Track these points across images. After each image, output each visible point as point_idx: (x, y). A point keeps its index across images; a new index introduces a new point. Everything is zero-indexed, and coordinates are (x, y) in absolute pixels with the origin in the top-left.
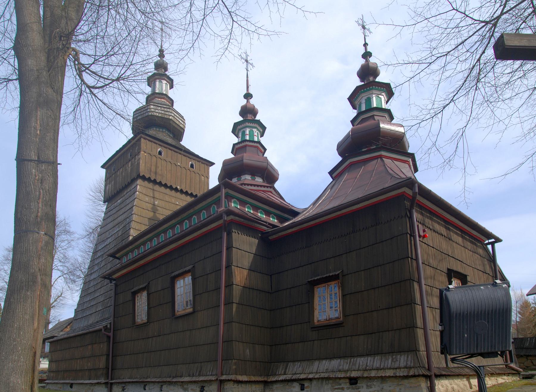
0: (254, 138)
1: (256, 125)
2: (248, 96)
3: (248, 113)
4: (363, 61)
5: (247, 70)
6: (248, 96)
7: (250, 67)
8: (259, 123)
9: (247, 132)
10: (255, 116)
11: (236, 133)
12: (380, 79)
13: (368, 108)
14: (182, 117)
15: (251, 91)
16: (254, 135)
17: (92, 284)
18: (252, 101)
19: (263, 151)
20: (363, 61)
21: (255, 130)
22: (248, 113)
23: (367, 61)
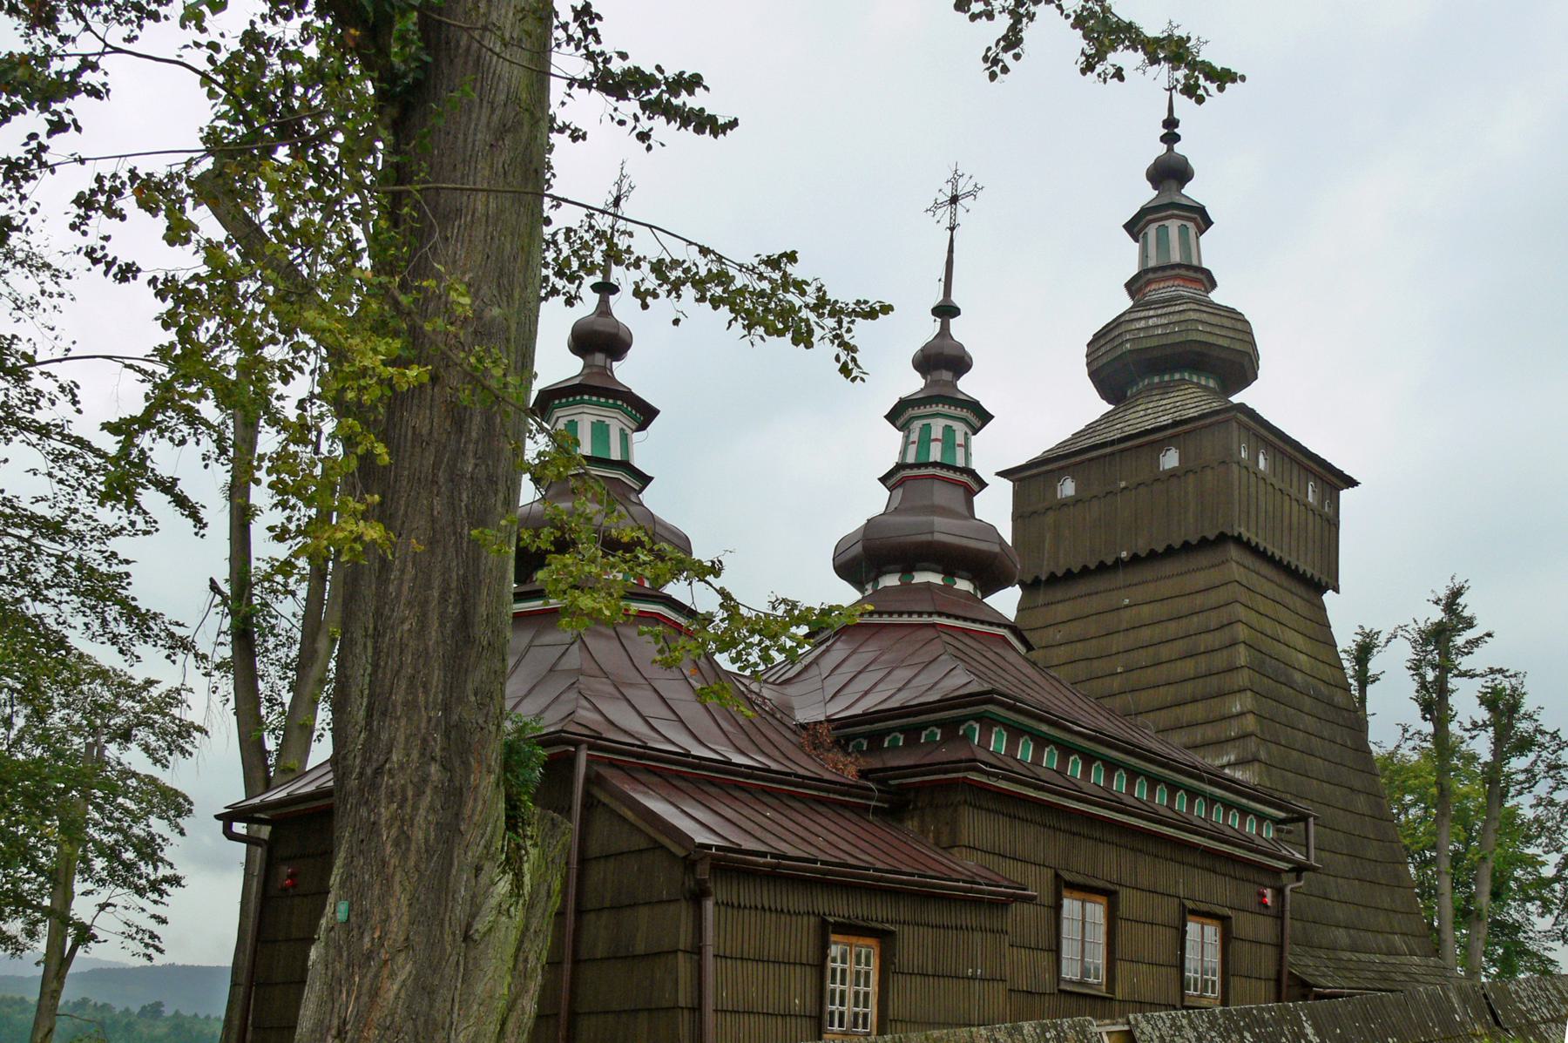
1: (964, 413)
2: (946, 311)
9: (937, 432)
13: (922, 460)
20: (933, 327)
23: (945, 331)
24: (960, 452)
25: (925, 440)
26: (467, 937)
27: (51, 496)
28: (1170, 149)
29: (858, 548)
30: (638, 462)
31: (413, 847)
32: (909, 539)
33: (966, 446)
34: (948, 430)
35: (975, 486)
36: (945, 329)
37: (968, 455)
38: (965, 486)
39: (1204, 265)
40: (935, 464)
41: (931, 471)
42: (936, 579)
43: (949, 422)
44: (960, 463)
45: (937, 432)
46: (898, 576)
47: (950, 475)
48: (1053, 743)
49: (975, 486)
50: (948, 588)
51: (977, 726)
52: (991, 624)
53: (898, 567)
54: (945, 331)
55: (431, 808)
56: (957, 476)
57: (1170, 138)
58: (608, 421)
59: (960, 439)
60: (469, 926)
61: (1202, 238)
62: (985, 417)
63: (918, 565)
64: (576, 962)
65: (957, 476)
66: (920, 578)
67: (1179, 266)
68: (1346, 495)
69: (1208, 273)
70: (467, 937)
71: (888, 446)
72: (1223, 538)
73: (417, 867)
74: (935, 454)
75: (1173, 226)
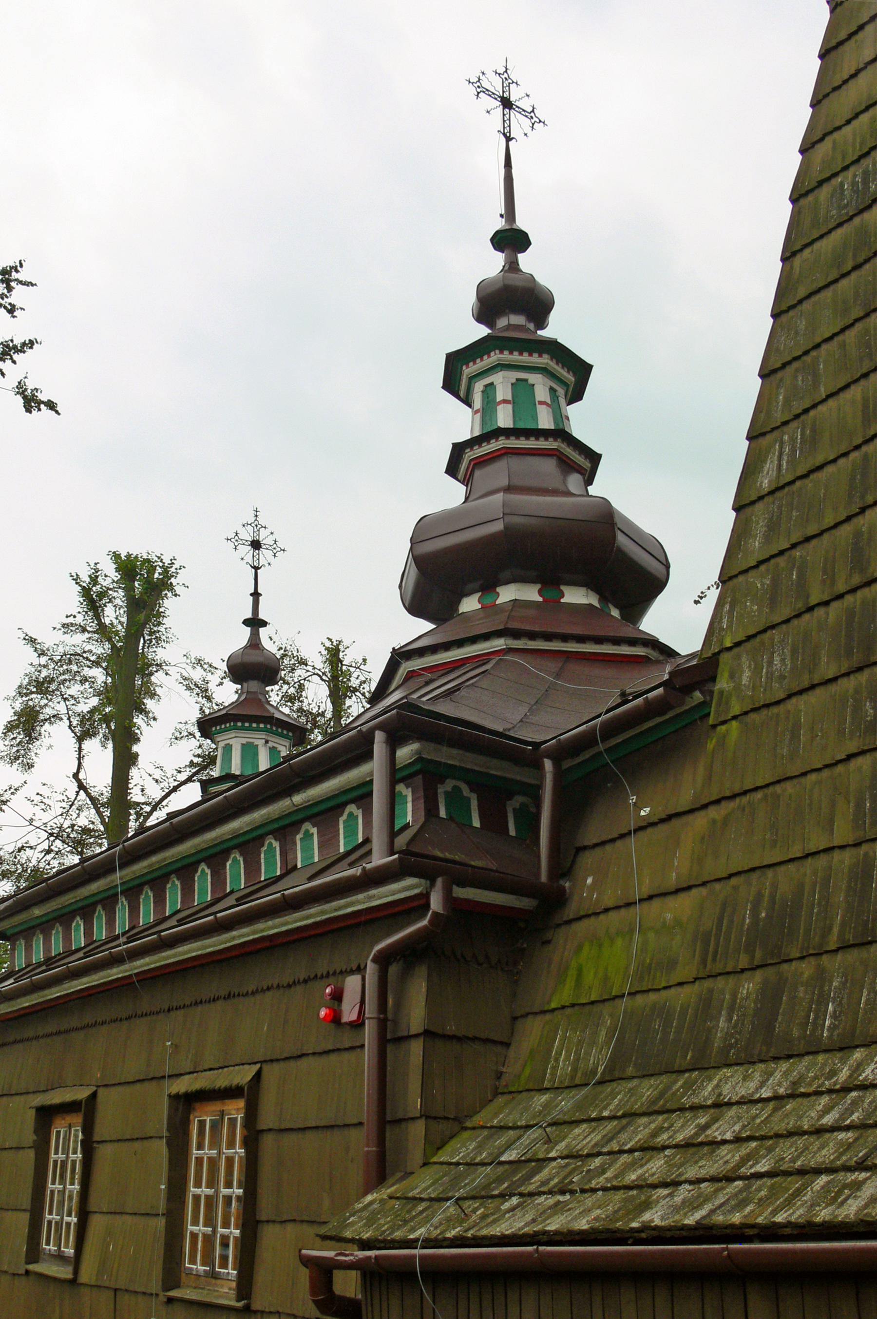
0: (535, 418)
1: (545, 360)
2: (511, 240)
3: (514, 306)
4: (494, 263)
5: (508, 139)
6: (511, 240)
7: (519, 124)
8: (558, 351)
9: (503, 392)
10: (541, 323)
11: (462, 394)
12: (555, 329)
13: (489, 429)
15: (522, 223)
16: (533, 403)
17: (724, 1130)
18: (525, 261)
19: (587, 464)
20: (494, 263)
21: (534, 378)
22: (514, 306)
23: (512, 266)
27: (362, 667)
29: (413, 572)
30: (578, 431)
42: (531, 593)
45: (503, 392)
46: (477, 596)
47: (532, 443)
48: (267, 834)
50: (552, 604)
51: (314, 830)
53: (476, 585)
54: (512, 266)
56: (542, 444)
63: (507, 574)
65: (542, 444)
66: (507, 594)
74: (504, 418)
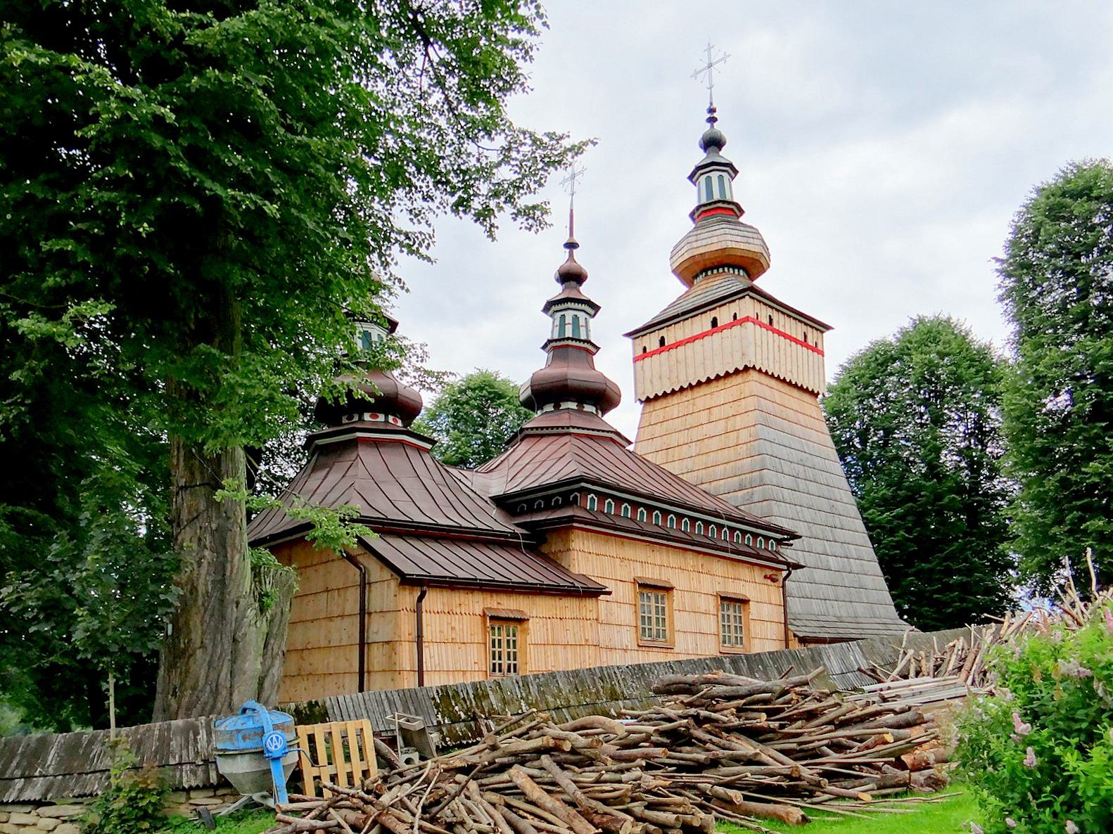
9: (569, 319)
14: (752, 228)
24: (583, 331)
25: (563, 324)
26: (234, 640)
28: (712, 126)
31: (200, 593)
32: (582, 383)
33: (587, 326)
34: (576, 318)
35: (593, 350)
36: (571, 255)
37: (587, 331)
38: (587, 350)
39: (735, 201)
40: (568, 339)
41: (577, 344)
43: (576, 313)
44: (583, 337)
45: (569, 319)
47: (577, 344)
49: (593, 350)
52: (608, 432)
55: (208, 573)
56: (581, 345)
57: (712, 120)
58: (370, 331)
59: (582, 322)
60: (235, 634)
61: (733, 183)
62: (596, 308)
64: (485, 644)
65: (581, 345)
67: (719, 202)
68: (827, 334)
69: (737, 205)
70: (234, 640)
71: (546, 327)
72: (746, 369)
73: (203, 605)
74: (569, 333)
75: (715, 175)
